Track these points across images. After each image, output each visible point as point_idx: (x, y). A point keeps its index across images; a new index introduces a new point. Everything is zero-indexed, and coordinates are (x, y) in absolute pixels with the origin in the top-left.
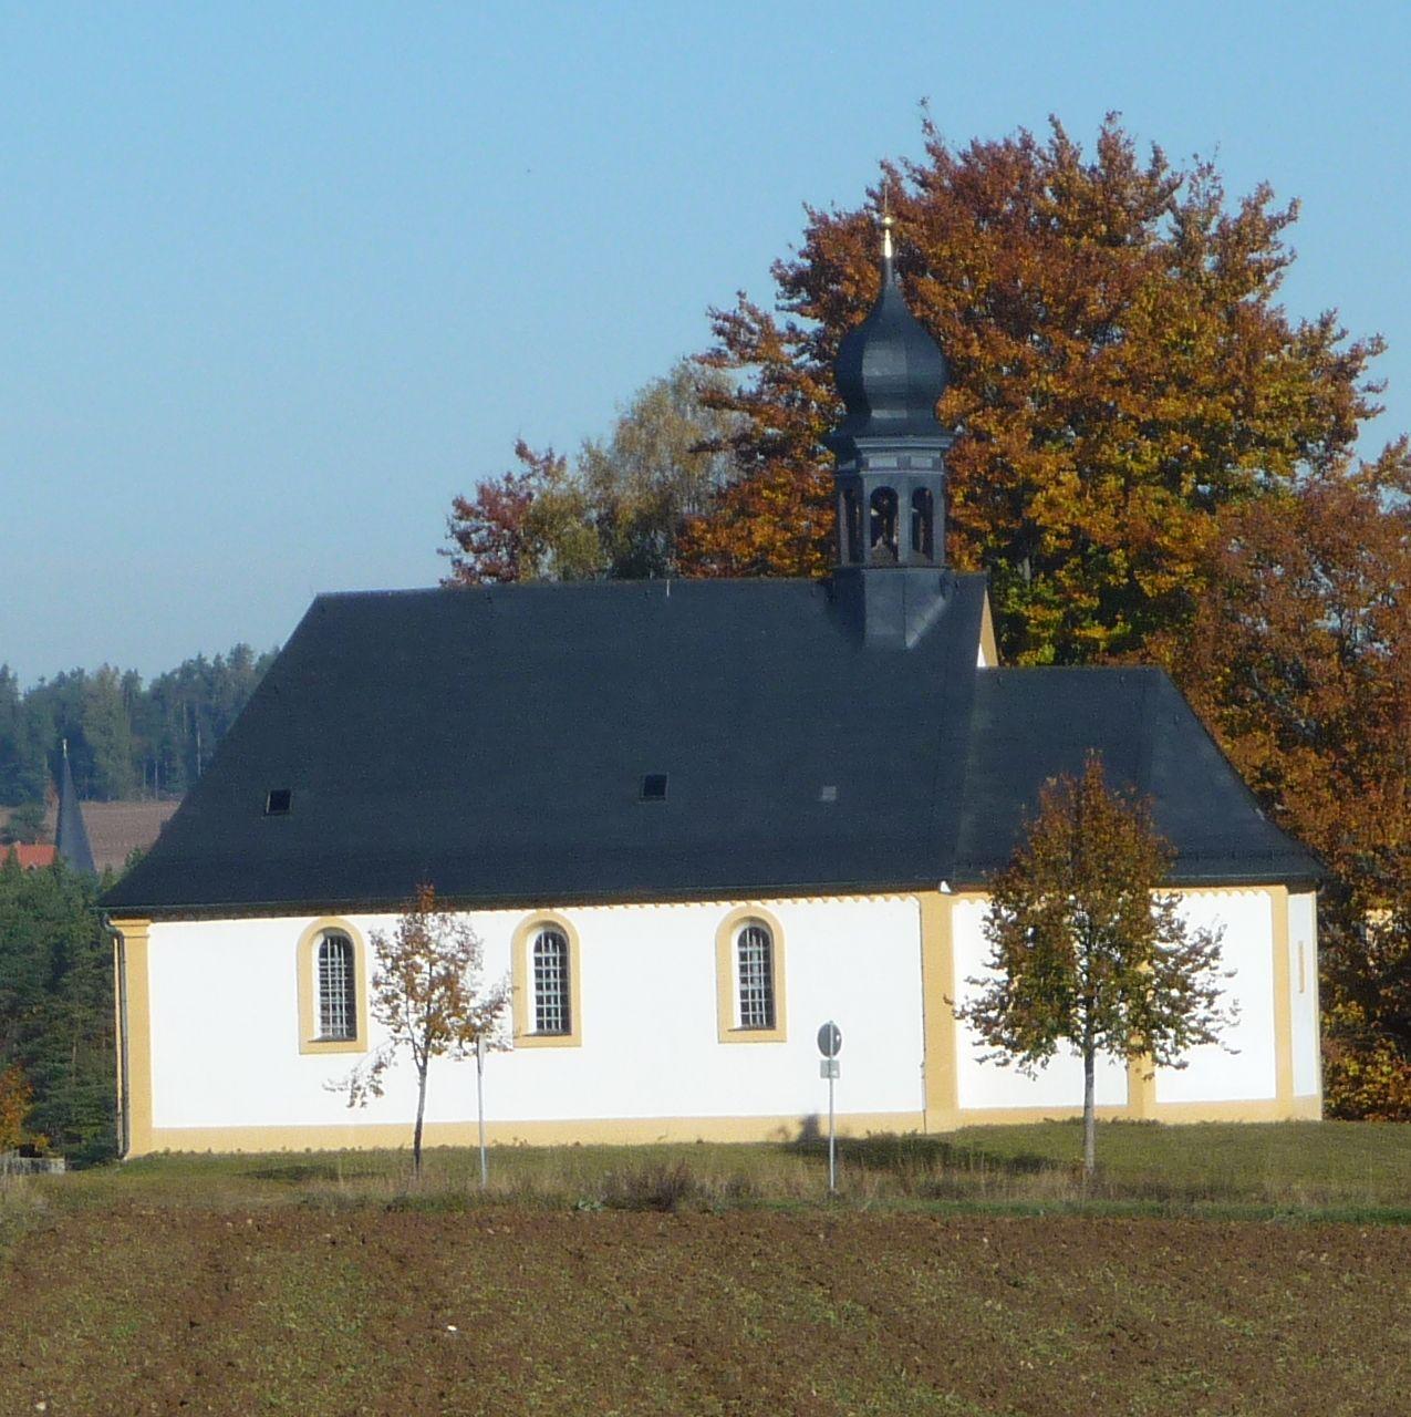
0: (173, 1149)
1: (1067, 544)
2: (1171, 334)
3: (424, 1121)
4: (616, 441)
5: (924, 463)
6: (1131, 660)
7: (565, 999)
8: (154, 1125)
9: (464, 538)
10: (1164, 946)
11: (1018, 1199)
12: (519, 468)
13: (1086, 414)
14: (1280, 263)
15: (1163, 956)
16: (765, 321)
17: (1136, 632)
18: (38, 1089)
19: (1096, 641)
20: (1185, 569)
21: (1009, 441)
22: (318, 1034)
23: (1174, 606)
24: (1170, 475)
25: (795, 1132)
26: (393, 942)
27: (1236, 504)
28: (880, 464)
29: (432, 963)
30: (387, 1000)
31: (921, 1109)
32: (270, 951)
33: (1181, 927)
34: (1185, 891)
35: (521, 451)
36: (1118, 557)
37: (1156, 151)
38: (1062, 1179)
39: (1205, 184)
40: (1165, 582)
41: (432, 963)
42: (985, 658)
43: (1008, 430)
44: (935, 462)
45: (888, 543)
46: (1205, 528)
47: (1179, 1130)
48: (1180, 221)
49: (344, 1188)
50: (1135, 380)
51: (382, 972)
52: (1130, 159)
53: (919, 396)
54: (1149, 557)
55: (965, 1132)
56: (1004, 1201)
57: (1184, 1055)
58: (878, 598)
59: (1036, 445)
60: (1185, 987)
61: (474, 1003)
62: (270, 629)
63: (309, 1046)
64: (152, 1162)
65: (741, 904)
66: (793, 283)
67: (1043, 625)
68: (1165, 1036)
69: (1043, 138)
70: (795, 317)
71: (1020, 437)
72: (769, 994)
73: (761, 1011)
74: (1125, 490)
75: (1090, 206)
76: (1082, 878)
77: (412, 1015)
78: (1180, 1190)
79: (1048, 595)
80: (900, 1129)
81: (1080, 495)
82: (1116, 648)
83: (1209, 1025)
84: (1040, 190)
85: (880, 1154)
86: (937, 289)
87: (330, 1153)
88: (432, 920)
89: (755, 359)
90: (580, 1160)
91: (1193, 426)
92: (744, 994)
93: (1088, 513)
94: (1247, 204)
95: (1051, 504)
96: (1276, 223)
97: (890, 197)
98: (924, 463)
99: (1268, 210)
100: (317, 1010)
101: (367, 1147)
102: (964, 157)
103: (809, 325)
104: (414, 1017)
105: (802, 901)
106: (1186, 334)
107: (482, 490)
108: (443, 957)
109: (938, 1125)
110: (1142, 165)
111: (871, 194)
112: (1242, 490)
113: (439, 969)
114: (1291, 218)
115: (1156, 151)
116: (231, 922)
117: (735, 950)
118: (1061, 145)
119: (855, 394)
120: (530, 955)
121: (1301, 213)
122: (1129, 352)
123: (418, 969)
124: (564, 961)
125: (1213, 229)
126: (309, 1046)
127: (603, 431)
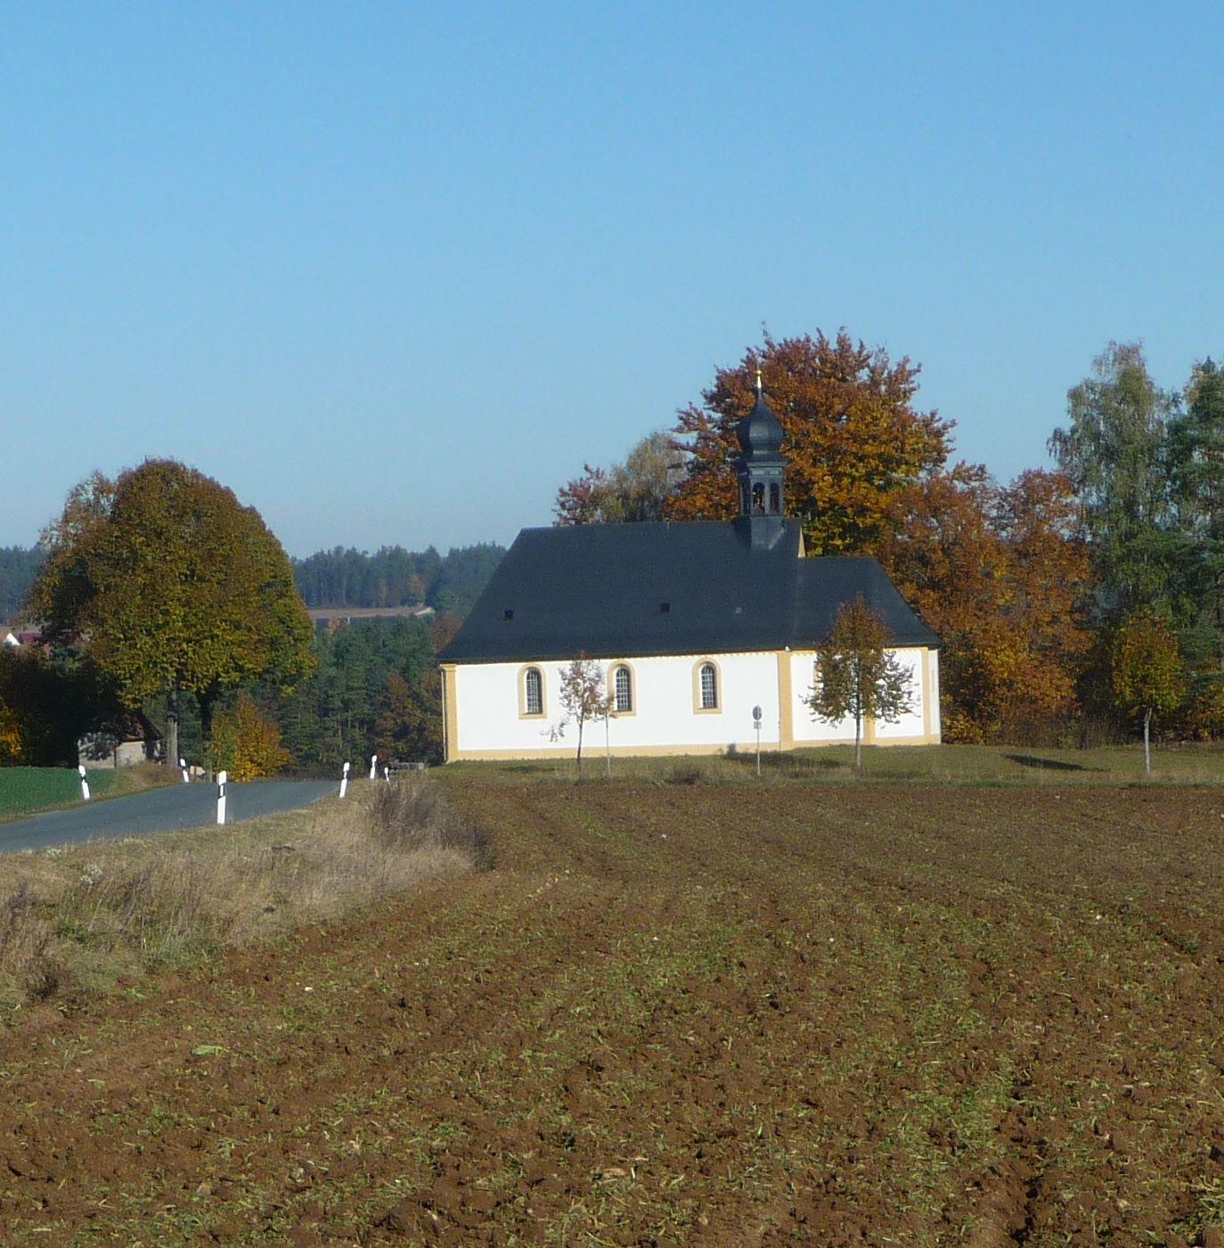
1: (827, 506)
2: (869, 419)
3: (582, 746)
4: (628, 464)
5: (775, 472)
6: (857, 554)
7: (629, 696)
9: (563, 505)
10: (889, 673)
11: (836, 777)
12: (586, 475)
13: (832, 452)
14: (914, 389)
15: (889, 677)
16: (700, 415)
17: (855, 542)
18: (285, 729)
19: (838, 546)
20: (877, 516)
21: (803, 463)
22: (526, 711)
23: (873, 530)
24: (868, 478)
25: (726, 751)
26: (568, 673)
27: (896, 489)
28: (757, 473)
29: (584, 682)
30: (566, 697)
31: (778, 740)
32: (507, 676)
33: (898, 664)
34: (896, 650)
35: (586, 468)
36: (849, 511)
37: (861, 343)
38: (848, 770)
39: (881, 356)
40: (869, 521)
41: (584, 682)
42: (801, 554)
43: (802, 459)
44: (780, 473)
45: (760, 506)
46: (884, 500)
47: (887, 749)
48: (872, 372)
49: (557, 775)
50: (855, 438)
51: (564, 686)
52: (850, 346)
53: (771, 445)
54: (862, 511)
55: (798, 750)
56: (823, 779)
57: (898, 718)
58: (757, 528)
59: (814, 465)
60: (899, 689)
61: (602, 698)
62: (507, 541)
63: (523, 716)
64: (458, 764)
65: (703, 656)
66: (711, 398)
67: (818, 539)
68: (890, 710)
69: (814, 338)
70: (711, 413)
71: (807, 462)
72: (715, 694)
73: (711, 701)
74: (852, 483)
75: (835, 366)
76: (856, 645)
77: (576, 704)
78: (894, 772)
79: (820, 527)
81: (832, 486)
82: (847, 548)
83: (908, 706)
84: (813, 358)
85: (773, 760)
86: (772, 400)
88: (584, 663)
89: (696, 430)
90: (657, 763)
91: (880, 456)
92: (704, 693)
93: (836, 493)
94: (899, 365)
95: (820, 489)
96: (911, 373)
97: (750, 361)
98: (775, 472)
99: (908, 367)
100: (526, 701)
102: (780, 345)
103: (717, 416)
104: (578, 704)
105: (728, 655)
106: (875, 418)
107: (570, 485)
108: (590, 679)
109: (786, 747)
110: (855, 349)
111: (742, 361)
112: (898, 484)
113: (587, 684)
114: (919, 371)
115: (861, 343)
117: (700, 675)
118: (822, 340)
119: (747, 445)
120: (615, 678)
121: (922, 369)
122: (852, 426)
123: (578, 684)
124: (629, 680)
125: (885, 375)
126: (523, 716)
127: (622, 460)
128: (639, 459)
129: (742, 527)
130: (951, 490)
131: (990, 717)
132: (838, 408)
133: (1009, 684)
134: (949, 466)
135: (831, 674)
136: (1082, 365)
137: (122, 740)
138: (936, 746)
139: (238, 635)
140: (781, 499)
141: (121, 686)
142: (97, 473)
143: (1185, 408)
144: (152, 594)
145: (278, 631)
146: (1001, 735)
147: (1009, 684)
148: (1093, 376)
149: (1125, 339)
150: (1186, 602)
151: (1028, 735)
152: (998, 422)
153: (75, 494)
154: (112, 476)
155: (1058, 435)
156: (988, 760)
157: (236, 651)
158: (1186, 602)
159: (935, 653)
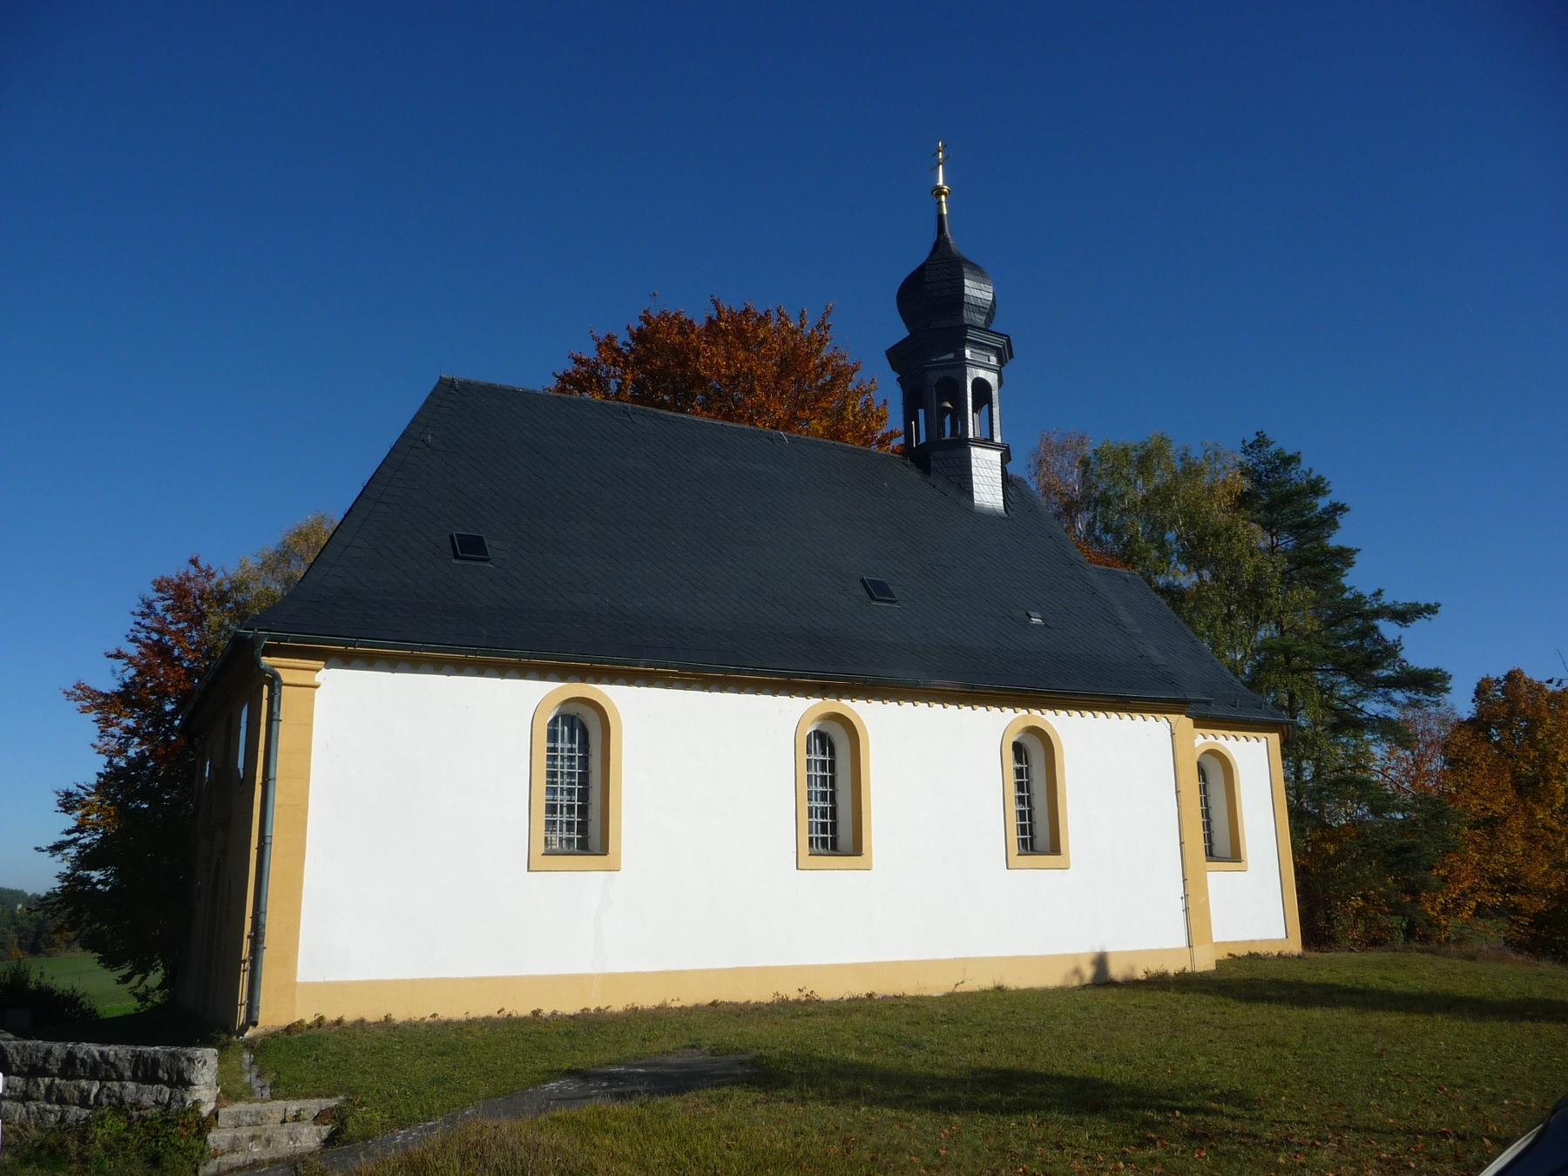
0: (330, 1016)
8: (298, 980)
25: (1088, 972)
80: (1172, 968)
87: (448, 1023)
101: (618, 1006)
116: (634, 688)
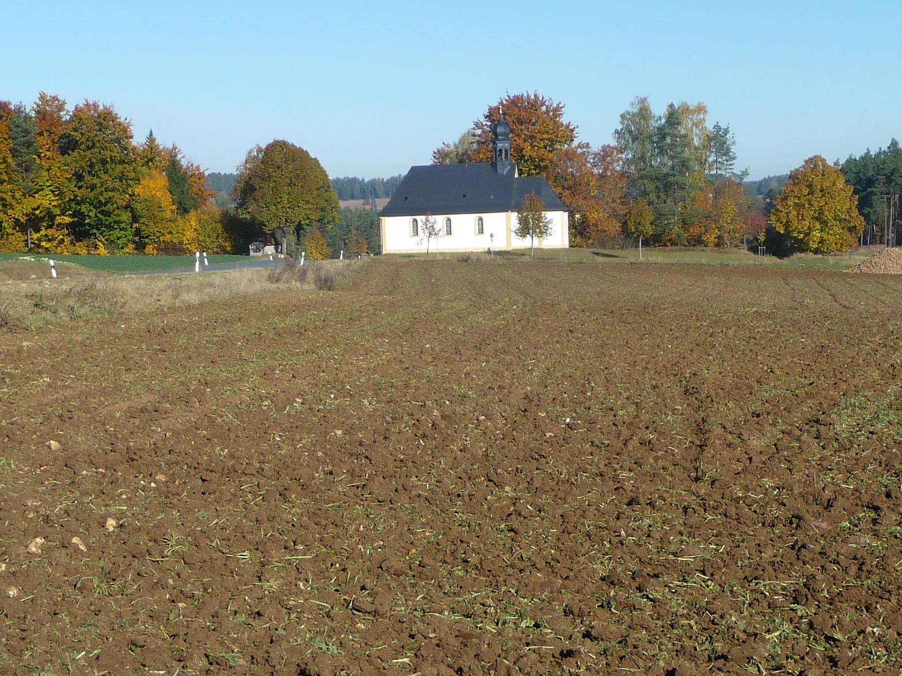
13: (532, 137)
21: (520, 142)
23: (546, 167)
28: (500, 145)
42: (516, 176)
46: (551, 155)
50: (539, 132)
54: (542, 160)
62: (404, 172)
63: (411, 237)
64: (386, 255)
69: (525, 94)
73: (481, 231)
91: (548, 139)
103: (489, 123)
110: (541, 98)
126: (411, 237)
128: (462, 140)
129: (494, 166)
130: (575, 152)
131: (589, 238)
132: (534, 121)
133: (596, 225)
134: (576, 143)
135: (524, 222)
136: (627, 106)
137: (266, 245)
138: (565, 249)
139: (308, 206)
140: (511, 155)
141: (265, 226)
142: (258, 145)
143: (663, 121)
144: (275, 190)
145: (324, 204)
146: (593, 244)
147: (596, 225)
148: (630, 110)
149: (642, 96)
150: (662, 195)
151: (603, 245)
152: (594, 126)
153: (250, 153)
154: (264, 146)
155: (616, 132)
156: (585, 254)
157: (308, 212)
158: (662, 195)
159: (566, 214)
